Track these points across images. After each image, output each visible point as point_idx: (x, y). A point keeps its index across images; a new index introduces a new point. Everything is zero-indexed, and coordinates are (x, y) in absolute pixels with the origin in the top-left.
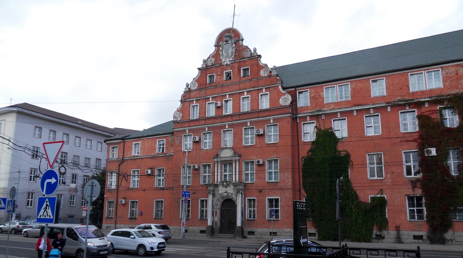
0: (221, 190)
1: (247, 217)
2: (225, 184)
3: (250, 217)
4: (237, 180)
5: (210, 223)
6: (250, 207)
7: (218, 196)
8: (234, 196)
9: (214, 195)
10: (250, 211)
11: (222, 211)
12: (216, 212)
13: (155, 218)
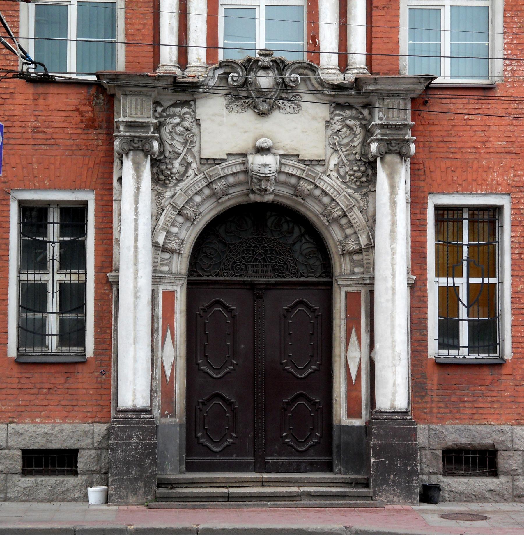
0: (222, 130)
1: (432, 348)
2: (265, 80)
3: (448, 334)
4: (358, 61)
5: (133, 389)
6: (448, 266)
7: (194, 180)
8: (331, 183)
9: (161, 178)
10: (448, 296)
11: (194, 287)
12: (169, 296)
13: (21, 362)
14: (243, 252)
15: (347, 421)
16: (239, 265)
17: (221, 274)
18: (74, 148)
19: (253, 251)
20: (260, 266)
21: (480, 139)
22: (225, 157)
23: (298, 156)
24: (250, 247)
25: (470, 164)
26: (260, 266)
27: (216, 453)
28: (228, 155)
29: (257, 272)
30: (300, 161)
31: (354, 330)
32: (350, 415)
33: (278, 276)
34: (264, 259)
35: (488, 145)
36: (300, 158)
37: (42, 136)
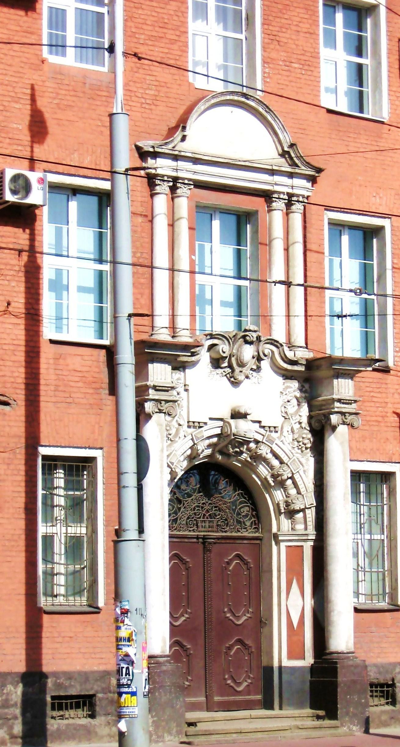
14: (194, 508)
15: (286, 663)
16: (192, 520)
17: (178, 528)
18: (88, 407)
19: (202, 508)
20: (207, 522)
21: (381, 414)
22: (207, 420)
23: (259, 422)
24: (199, 504)
25: (375, 436)
26: (207, 522)
27: (240, 692)
28: (211, 419)
29: (212, 527)
30: (261, 427)
31: (295, 581)
32: (291, 656)
33: (223, 532)
34: (210, 515)
35: (386, 419)
36: (263, 424)
37: (61, 394)
